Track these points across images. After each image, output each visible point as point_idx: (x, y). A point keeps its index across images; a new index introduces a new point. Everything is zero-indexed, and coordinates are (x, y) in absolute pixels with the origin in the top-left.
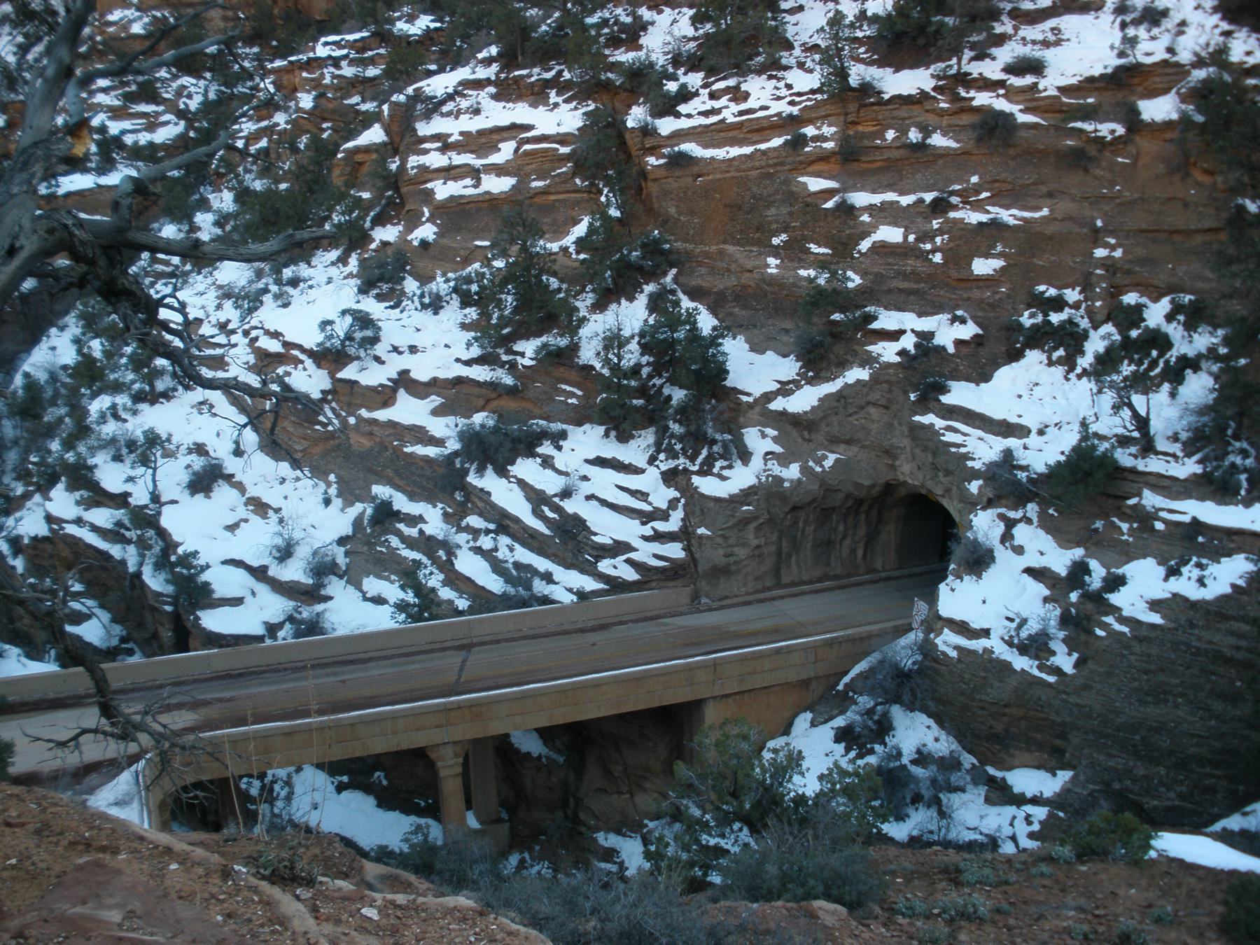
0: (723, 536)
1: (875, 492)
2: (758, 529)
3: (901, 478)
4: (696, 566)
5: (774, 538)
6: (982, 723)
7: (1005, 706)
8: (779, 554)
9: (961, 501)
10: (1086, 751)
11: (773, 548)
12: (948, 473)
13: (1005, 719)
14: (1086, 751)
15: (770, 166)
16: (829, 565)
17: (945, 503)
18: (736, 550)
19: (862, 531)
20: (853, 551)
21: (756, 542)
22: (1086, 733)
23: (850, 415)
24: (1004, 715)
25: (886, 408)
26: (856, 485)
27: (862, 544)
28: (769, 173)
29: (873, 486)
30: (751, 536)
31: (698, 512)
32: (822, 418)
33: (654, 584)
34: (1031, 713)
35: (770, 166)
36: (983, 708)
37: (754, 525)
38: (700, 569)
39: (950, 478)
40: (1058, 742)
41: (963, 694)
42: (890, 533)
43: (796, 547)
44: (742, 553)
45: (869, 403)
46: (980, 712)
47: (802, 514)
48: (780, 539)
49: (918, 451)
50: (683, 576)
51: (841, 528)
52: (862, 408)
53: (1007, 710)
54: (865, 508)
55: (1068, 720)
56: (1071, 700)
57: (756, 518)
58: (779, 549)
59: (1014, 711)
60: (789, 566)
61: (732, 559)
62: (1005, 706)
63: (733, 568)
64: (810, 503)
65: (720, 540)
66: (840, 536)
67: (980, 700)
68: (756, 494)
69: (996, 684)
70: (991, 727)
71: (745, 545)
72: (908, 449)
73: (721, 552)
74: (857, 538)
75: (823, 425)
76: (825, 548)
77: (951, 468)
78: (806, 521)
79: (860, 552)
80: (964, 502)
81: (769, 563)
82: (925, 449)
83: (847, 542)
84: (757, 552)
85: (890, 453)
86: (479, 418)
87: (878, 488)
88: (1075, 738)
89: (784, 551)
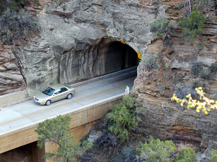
0: (36, 67)
1: (97, 42)
2: (51, 62)
3: (109, 35)
4: (25, 81)
5: (57, 66)
6: (163, 134)
7: (173, 126)
8: (59, 72)
9: (138, 42)
10: (210, 141)
11: (57, 70)
12: (131, 31)
13: (173, 131)
14: (210, 141)
16: (79, 75)
17: (131, 44)
18: (42, 72)
19: (91, 59)
20: (88, 68)
21: (50, 68)
22: (209, 133)
23: (85, 10)
24: (173, 129)
25: (101, 6)
26: (92, 40)
27: (92, 65)
29: (96, 40)
30: (48, 66)
31: (24, 57)
32: (73, 12)
33: (8, 91)
34: (185, 127)
36: (163, 128)
37: (49, 60)
38: (27, 82)
39: (133, 33)
40: (197, 139)
41: (153, 123)
42: (102, 58)
43: (65, 69)
44: (44, 73)
45: (93, 4)
46: (162, 130)
47: (68, 54)
48: (59, 66)
49: (117, 23)
50: (21, 86)
51: (83, 59)
52: (90, 6)
53: (174, 128)
54: (92, 49)
55: (201, 129)
56: (201, 120)
57: (50, 58)
58: (59, 70)
59: (177, 127)
60: (63, 77)
61: (41, 76)
62: (173, 126)
63: (41, 80)
64: (71, 49)
65: (34, 69)
66: (83, 62)
67: (162, 125)
68: (48, 47)
69: (168, 117)
70: (168, 135)
71: (45, 70)
72: (112, 23)
73: (36, 74)
74: (90, 63)
75: (73, 15)
76: (77, 67)
77: (133, 29)
78: (69, 57)
79: (91, 69)
80: (140, 43)
81: (55, 76)
82: (120, 22)
83: (85, 65)
84: (50, 73)
85: (104, 25)
86: (21, 7)
87: (99, 41)
88: (205, 136)
89: (61, 71)
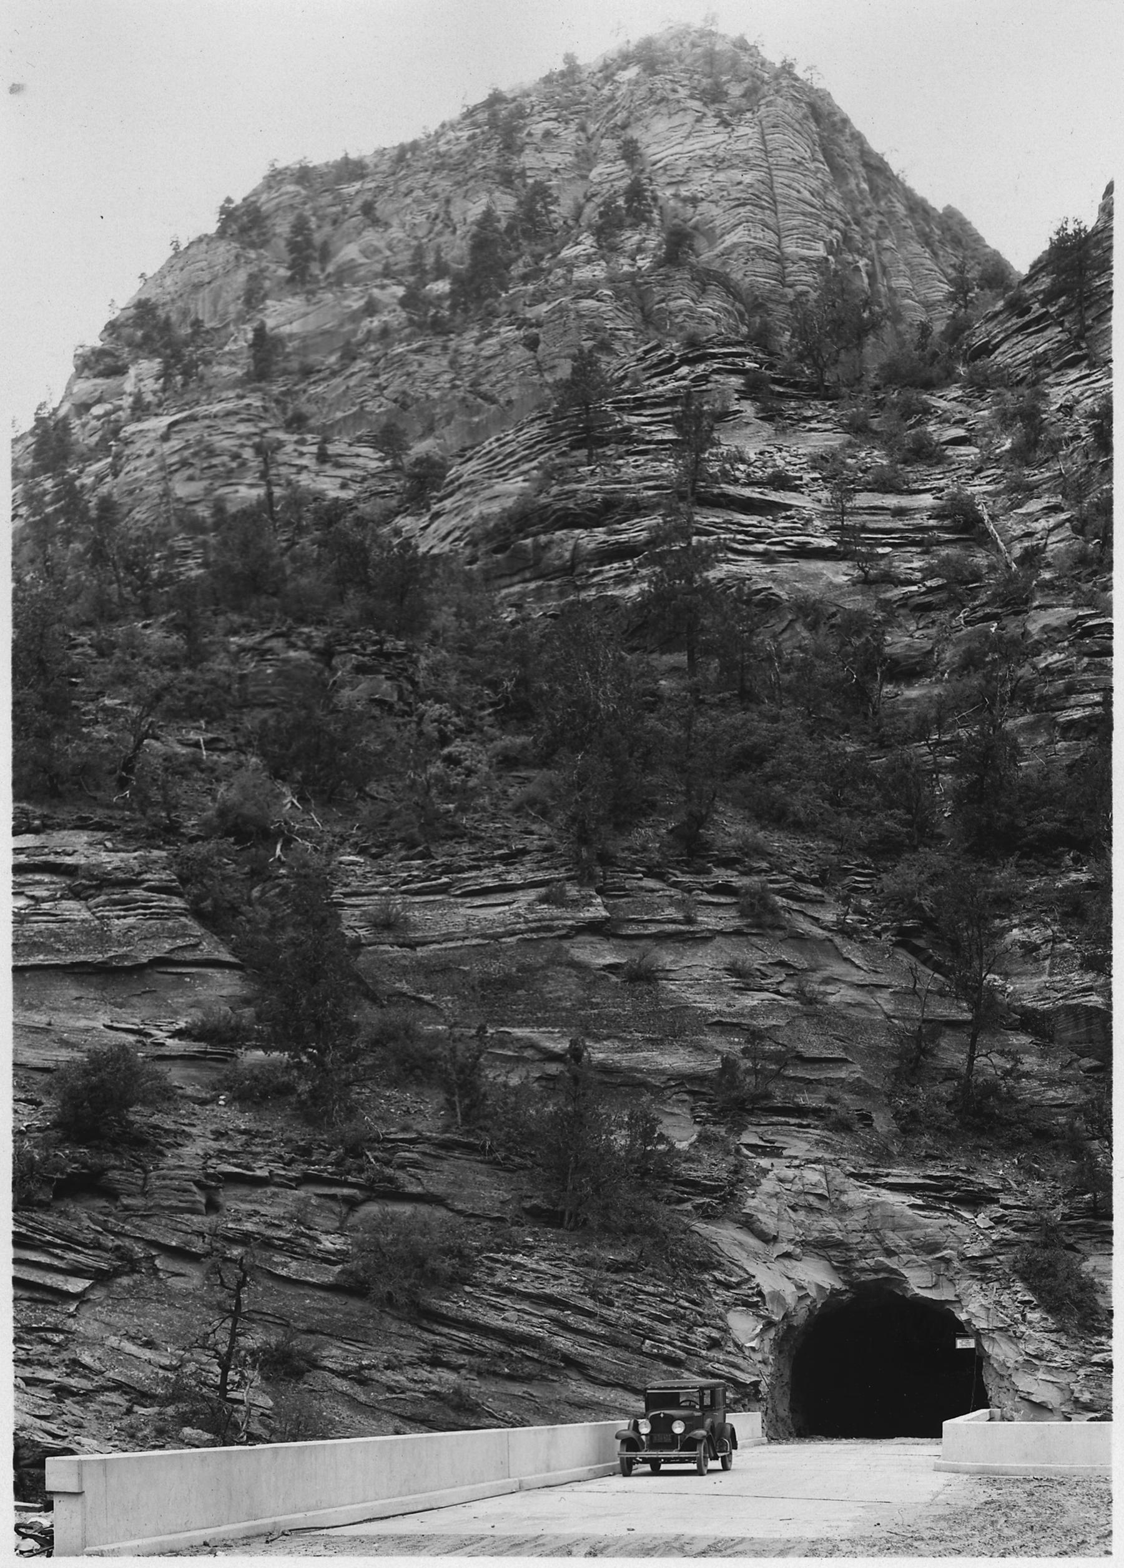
15: (532, 930)
28: (532, 940)
35: (532, 930)
